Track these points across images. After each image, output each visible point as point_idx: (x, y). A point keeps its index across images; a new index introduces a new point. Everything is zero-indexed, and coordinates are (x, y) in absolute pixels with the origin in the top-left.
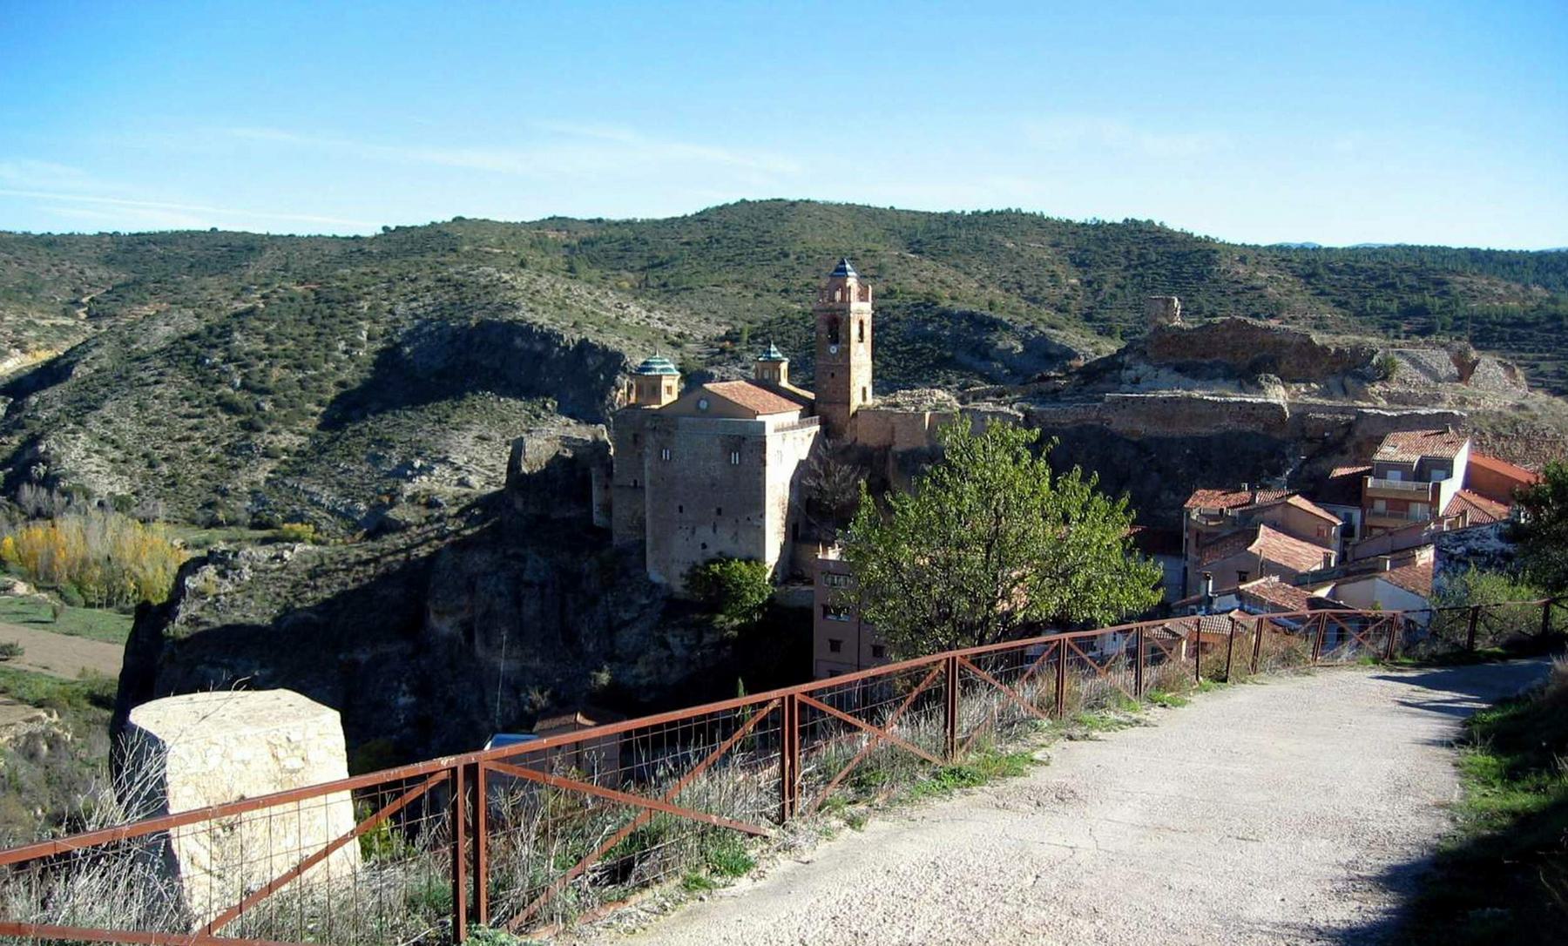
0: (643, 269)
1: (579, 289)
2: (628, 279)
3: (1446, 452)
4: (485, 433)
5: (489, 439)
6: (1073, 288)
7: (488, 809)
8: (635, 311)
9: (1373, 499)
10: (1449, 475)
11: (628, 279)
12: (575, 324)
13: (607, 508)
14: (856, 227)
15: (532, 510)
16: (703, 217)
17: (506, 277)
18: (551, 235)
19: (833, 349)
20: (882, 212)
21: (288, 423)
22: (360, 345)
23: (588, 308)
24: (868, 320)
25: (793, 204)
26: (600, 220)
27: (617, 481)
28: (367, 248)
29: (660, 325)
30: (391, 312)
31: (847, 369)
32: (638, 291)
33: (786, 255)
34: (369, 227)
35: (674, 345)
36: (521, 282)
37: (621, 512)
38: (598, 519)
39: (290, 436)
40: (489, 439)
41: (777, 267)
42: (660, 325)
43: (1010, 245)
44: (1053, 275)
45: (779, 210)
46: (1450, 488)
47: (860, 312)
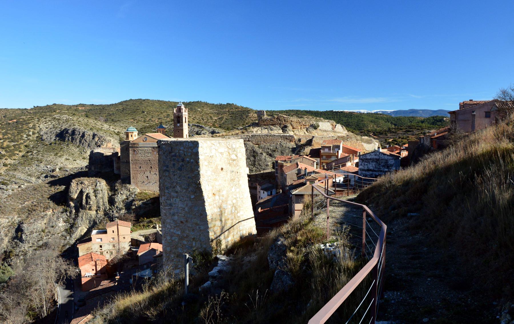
0: (106, 116)
1: (91, 121)
2: (103, 119)
3: (338, 144)
4: (68, 158)
5: (69, 159)
6: (216, 120)
7: (373, 180)
8: (106, 126)
9: (322, 156)
10: (339, 149)
11: (103, 119)
12: (91, 129)
13: (119, 168)
14: (160, 106)
15: (96, 170)
16: (121, 103)
17: (71, 117)
18: (80, 108)
19: (178, 125)
20: (167, 102)
21: (10, 156)
22: (30, 136)
23: (94, 125)
24: (187, 117)
25: (144, 100)
26: (93, 105)
27: (121, 161)
28: (29, 111)
29: (113, 130)
30: (39, 127)
31: (182, 130)
32: (106, 121)
33: (144, 112)
34: (29, 106)
35: (117, 134)
36: (75, 119)
37: (123, 168)
38: (116, 172)
39: (10, 160)
40: (69, 159)
41: (141, 115)
42: (113, 130)
43: (199, 110)
44: (211, 117)
45: (141, 101)
46: (340, 152)
47: (185, 115)
